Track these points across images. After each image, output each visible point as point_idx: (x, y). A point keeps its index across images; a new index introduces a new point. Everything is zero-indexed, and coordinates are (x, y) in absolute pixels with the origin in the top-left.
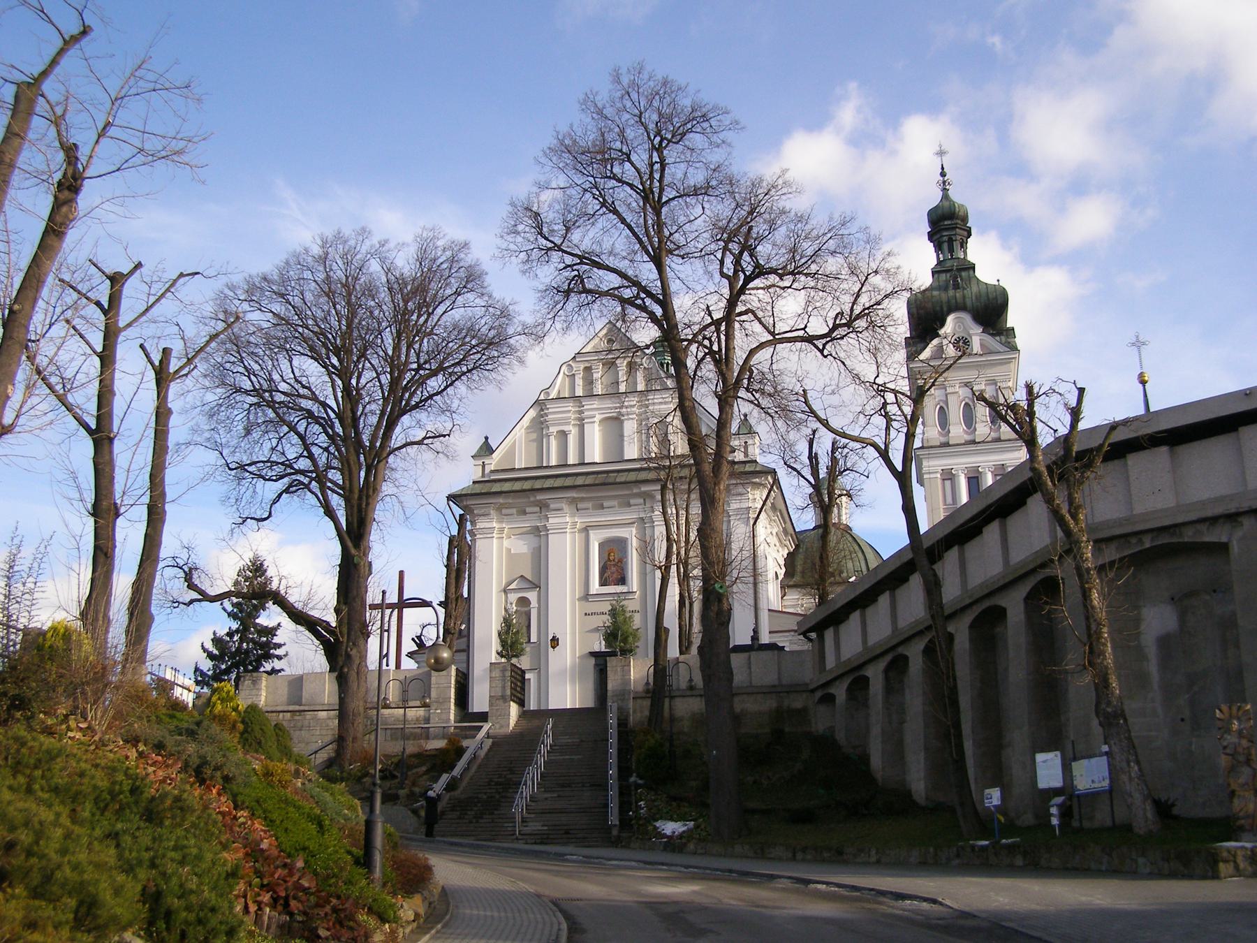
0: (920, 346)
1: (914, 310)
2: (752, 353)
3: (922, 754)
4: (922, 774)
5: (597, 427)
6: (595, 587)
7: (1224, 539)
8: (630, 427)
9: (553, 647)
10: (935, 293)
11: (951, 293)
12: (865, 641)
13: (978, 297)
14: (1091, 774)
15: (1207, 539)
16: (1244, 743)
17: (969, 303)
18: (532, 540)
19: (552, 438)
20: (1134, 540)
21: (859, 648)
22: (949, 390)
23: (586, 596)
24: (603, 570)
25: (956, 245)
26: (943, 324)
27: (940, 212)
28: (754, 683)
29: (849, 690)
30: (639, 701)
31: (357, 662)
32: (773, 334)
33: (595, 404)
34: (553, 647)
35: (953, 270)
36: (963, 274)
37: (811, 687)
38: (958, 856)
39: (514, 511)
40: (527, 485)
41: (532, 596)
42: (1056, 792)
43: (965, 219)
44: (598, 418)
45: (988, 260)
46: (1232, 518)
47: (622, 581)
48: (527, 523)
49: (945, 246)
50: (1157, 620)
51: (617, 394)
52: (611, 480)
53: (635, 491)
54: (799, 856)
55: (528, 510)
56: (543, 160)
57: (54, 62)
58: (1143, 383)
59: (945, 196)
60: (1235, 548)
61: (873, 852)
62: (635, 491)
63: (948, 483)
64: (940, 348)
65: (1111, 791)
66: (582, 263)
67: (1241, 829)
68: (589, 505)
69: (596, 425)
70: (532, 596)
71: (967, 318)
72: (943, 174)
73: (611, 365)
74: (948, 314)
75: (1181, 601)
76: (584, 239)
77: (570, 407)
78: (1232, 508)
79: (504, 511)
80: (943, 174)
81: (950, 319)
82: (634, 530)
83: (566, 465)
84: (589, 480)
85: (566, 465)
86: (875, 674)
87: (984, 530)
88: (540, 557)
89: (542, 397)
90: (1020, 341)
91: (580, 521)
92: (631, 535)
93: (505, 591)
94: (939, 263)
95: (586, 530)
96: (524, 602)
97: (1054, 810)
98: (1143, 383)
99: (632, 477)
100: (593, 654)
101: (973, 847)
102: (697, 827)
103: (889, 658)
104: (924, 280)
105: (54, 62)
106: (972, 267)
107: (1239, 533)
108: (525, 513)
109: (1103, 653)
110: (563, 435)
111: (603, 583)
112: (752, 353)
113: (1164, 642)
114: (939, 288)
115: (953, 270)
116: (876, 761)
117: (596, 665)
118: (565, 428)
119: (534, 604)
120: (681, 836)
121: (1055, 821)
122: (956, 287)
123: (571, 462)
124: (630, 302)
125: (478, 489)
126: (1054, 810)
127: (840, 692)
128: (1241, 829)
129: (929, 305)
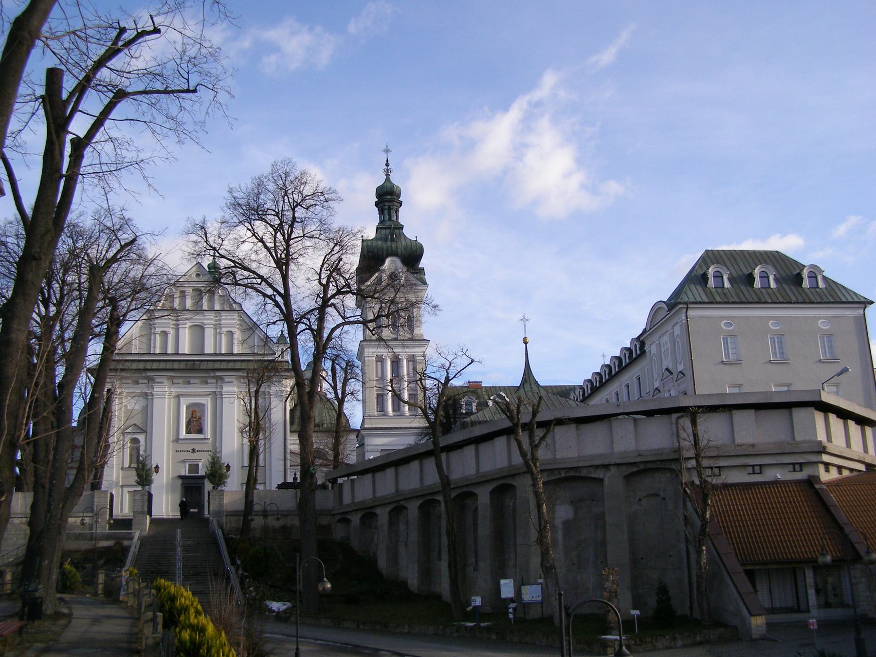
0: (367, 275)
1: (365, 252)
2: (333, 330)
3: (416, 566)
4: (416, 575)
5: (187, 331)
6: (183, 434)
7: (601, 477)
8: (209, 333)
9: (157, 472)
10: (380, 243)
11: (389, 243)
12: (374, 492)
13: (406, 248)
14: (532, 593)
15: (593, 476)
16: (615, 586)
17: (399, 251)
18: (142, 402)
19: (157, 336)
20: (556, 472)
21: (371, 496)
23: (177, 440)
24: (188, 423)
25: (393, 212)
26: (383, 262)
27: (385, 190)
29: (362, 518)
32: (343, 318)
34: (157, 472)
35: (389, 226)
36: (396, 231)
38: (457, 631)
40: (141, 366)
41: (141, 437)
42: (512, 600)
43: (399, 196)
44: (189, 324)
45: (412, 223)
46: (606, 467)
47: (200, 431)
48: (138, 389)
49: (386, 212)
50: (563, 512)
52: (197, 367)
53: (212, 375)
54: (361, 627)
55: (140, 381)
56: (225, 209)
58: (526, 343)
59: (388, 179)
60: (606, 481)
61: (406, 627)
62: (212, 375)
63: (379, 363)
64: (380, 280)
65: (542, 602)
66: (235, 266)
67: (612, 628)
68: (181, 381)
70: (141, 437)
72: (387, 165)
74: (386, 257)
75: (575, 503)
78: (607, 462)
79: (124, 381)
80: (387, 165)
81: (388, 261)
82: (209, 400)
83: (167, 354)
85: (167, 354)
86: (383, 514)
88: (147, 412)
90: (428, 278)
91: (175, 390)
93: (123, 434)
94: (381, 222)
95: (178, 397)
96: (135, 441)
97: (511, 610)
98: (526, 343)
99: (210, 366)
100: (181, 477)
101: (466, 627)
102: (294, 607)
103: (393, 506)
104: (371, 233)
106: (401, 227)
107: (609, 474)
108: (138, 383)
109: (546, 537)
110: (165, 334)
111: (188, 431)
112: (333, 330)
113: (567, 524)
114: (381, 239)
115: (389, 226)
116: (382, 563)
117: (182, 484)
118: (166, 329)
119: (142, 442)
120: (285, 611)
121: (511, 616)
122: (392, 240)
123: (169, 352)
124: (270, 297)
126: (511, 610)
127: (356, 519)
128: (612, 628)
129: (376, 250)
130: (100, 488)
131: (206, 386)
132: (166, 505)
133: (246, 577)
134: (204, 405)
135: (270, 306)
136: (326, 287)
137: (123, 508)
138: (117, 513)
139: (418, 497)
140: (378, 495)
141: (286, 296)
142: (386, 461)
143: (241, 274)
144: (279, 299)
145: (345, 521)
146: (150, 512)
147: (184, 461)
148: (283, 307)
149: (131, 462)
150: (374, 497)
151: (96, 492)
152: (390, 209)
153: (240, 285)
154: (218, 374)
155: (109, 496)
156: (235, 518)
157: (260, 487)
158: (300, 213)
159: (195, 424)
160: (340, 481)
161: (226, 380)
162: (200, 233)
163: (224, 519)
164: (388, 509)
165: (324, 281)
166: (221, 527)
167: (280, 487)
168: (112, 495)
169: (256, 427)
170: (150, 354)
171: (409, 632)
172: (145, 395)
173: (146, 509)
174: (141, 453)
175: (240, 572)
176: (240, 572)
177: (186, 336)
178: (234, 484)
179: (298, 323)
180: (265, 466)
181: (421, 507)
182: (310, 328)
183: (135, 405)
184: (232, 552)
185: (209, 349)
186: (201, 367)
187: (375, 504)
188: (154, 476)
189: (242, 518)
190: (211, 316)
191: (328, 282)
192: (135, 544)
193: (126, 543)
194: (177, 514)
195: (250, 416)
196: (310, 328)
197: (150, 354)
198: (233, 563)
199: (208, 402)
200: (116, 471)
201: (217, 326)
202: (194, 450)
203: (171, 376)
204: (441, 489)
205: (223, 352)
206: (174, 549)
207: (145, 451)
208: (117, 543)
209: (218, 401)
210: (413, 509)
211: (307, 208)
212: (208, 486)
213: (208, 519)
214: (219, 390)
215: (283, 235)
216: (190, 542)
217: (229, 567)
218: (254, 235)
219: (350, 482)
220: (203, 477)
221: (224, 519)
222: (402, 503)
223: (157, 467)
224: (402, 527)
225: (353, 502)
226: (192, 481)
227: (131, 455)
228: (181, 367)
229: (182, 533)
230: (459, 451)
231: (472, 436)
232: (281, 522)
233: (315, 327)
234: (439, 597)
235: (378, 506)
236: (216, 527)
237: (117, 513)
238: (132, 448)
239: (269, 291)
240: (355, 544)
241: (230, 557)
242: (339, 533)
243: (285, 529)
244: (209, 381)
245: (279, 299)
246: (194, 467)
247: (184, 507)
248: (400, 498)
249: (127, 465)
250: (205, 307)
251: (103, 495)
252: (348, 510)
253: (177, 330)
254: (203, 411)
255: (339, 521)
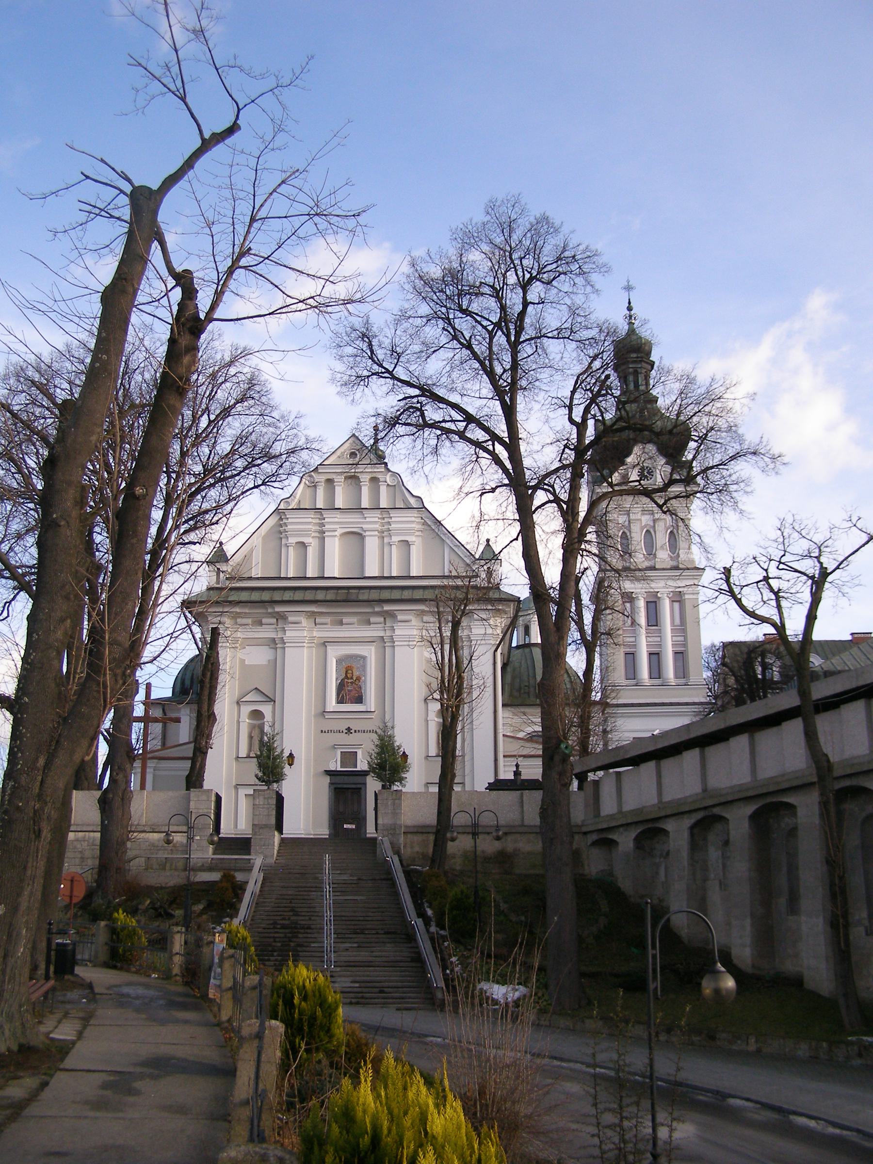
3: (748, 922)
4: (748, 940)
6: (332, 704)
8: (372, 544)
9: (290, 765)
19: (291, 549)
22: (632, 517)
24: (340, 687)
26: (628, 454)
28: (526, 823)
29: (637, 839)
30: (409, 836)
31: (123, 786)
33: (338, 517)
34: (290, 765)
37: (584, 829)
38: (860, 1055)
39: (249, 621)
40: (266, 596)
43: (649, 353)
47: (359, 700)
51: (360, 509)
52: (353, 597)
53: (377, 609)
55: (264, 621)
57: (189, 164)
60: (801, 812)
61: (752, 1040)
68: (328, 620)
69: (337, 539)
70: (266, 709)
71: (651, 448)
72: (630, 309)
73: (353, 479)
76: (434, 369)
77: (310, 518)
80: (630, 309)
81: (637, 450)
82: (373, 648)
84: (330, 596)
86: (678, 832)
87: (842, 706)
88: (275, 669)
89: (282, 506)
92: (370, 652)
95: (324, 644)
96: (257, 715)
100: (328, 773)
103: (699, 815)
105: (189, 164)
110: (303, 545)
111: (340, 700)
117: (331, 784)
119: (268, 717)
123: (309, 574)
125: (214, 596)
127: (626, 841)
130: (201, 786)
131: (367, 627)
132: (305, 812)
133: (444, 938)
134: (364, 658)
135: (485, 460)
136: (581, 427)
137: (237, 821)
138: (227, 829)
139: (748, 799)
140: (667, 797)
141: (513, 446)
142: (684, 737)
143: (433, 413)
144: (500, 450)
145: (606, 843)
146: (279, 827)
147: (334, 747)
148: (509, 466)
149: (250, 750)
150: (660, 801)
151: (194, 793)
152: (636, 373)
153: (454, 329)
154: (387, 608)
155: (213, 798)
156: (417, 838)
157: (457, 788)
158: (536, 291)
159: (350, 689)
160: (591, 776)
161: (400, 617)
162: (359, 343)
163: (402, 839)
164: (688, 822)
165: (577, 417)
166: (397, 852)
167: (492, 787)
168: (218, 799)
169: (451, 692)
170: (280, 578)
171: (759, 1051)
172: (273, 643)
173: (273, 821)
174: (267, 729)
175: (433, 929)
176: (433, 929)
177: (334, 548)
178: (419, 778)
179: (535, 488)
180: (463, 756)
181: (753, 817)
182: (557, 500)
183: (258, 656)
184: (417, 894)
185: (372, 569)
186: (361, 597)
187: (663, 814)
188: (287, 769)
189: (432, 837)
190: (374, 517)
191: (584, 419)
192: (254, 882)
193: (239, 877)
194: (324, 831)
195: (441, 670)
196: (557, 500)
197: (280, 578)
198: (421, 914)
199: (370, 652)
200: (225, 765)
201: (384, 534)
202: (349, 729)
203: (313, 612)
204: (815, 779)
205: (394, 574)
206: (320, 889)
207: (273, 726)
208: (224, 876)
209: (388, 651)
210: (739, 821)
211: (549, 283)
212: (373, 785)
213: (375, 839)
214: (388, 633)
215: (508, 336)
216: (345, 877)
217: (417, 923)
218: (455, 337)
219: (613, 778)
220: (364, 774)
221: (402, 839)
222: (716, 811)
223: (291, 756)
224: (714, 854)
225: (620, 812)
226: (346, 779)
227: (251, 737)
228: (329, 598)
229: (332, 861)
230: (774, 730)
231: (861, 683)
232: (497, 845)
233: (564, 496)
234: (797, 982)
235: (667, 817)
236: (390, 852)
237: (227, 829)
238: (252, 727)
239: (479, 435)
240: (626, 885)
241: (415, 902)
242: (594, 864)
243: (503, 858)
244: (372, 620)
245: (500, 450)
246: (349, 757)
247: (336, 819)
248: (710, 802)
249: (243, 753)
250: (365, 503)
251: (204, 797)
252: (613, 824)
253: (322, 540)
254: (364, 667)
255: (595, 843)
